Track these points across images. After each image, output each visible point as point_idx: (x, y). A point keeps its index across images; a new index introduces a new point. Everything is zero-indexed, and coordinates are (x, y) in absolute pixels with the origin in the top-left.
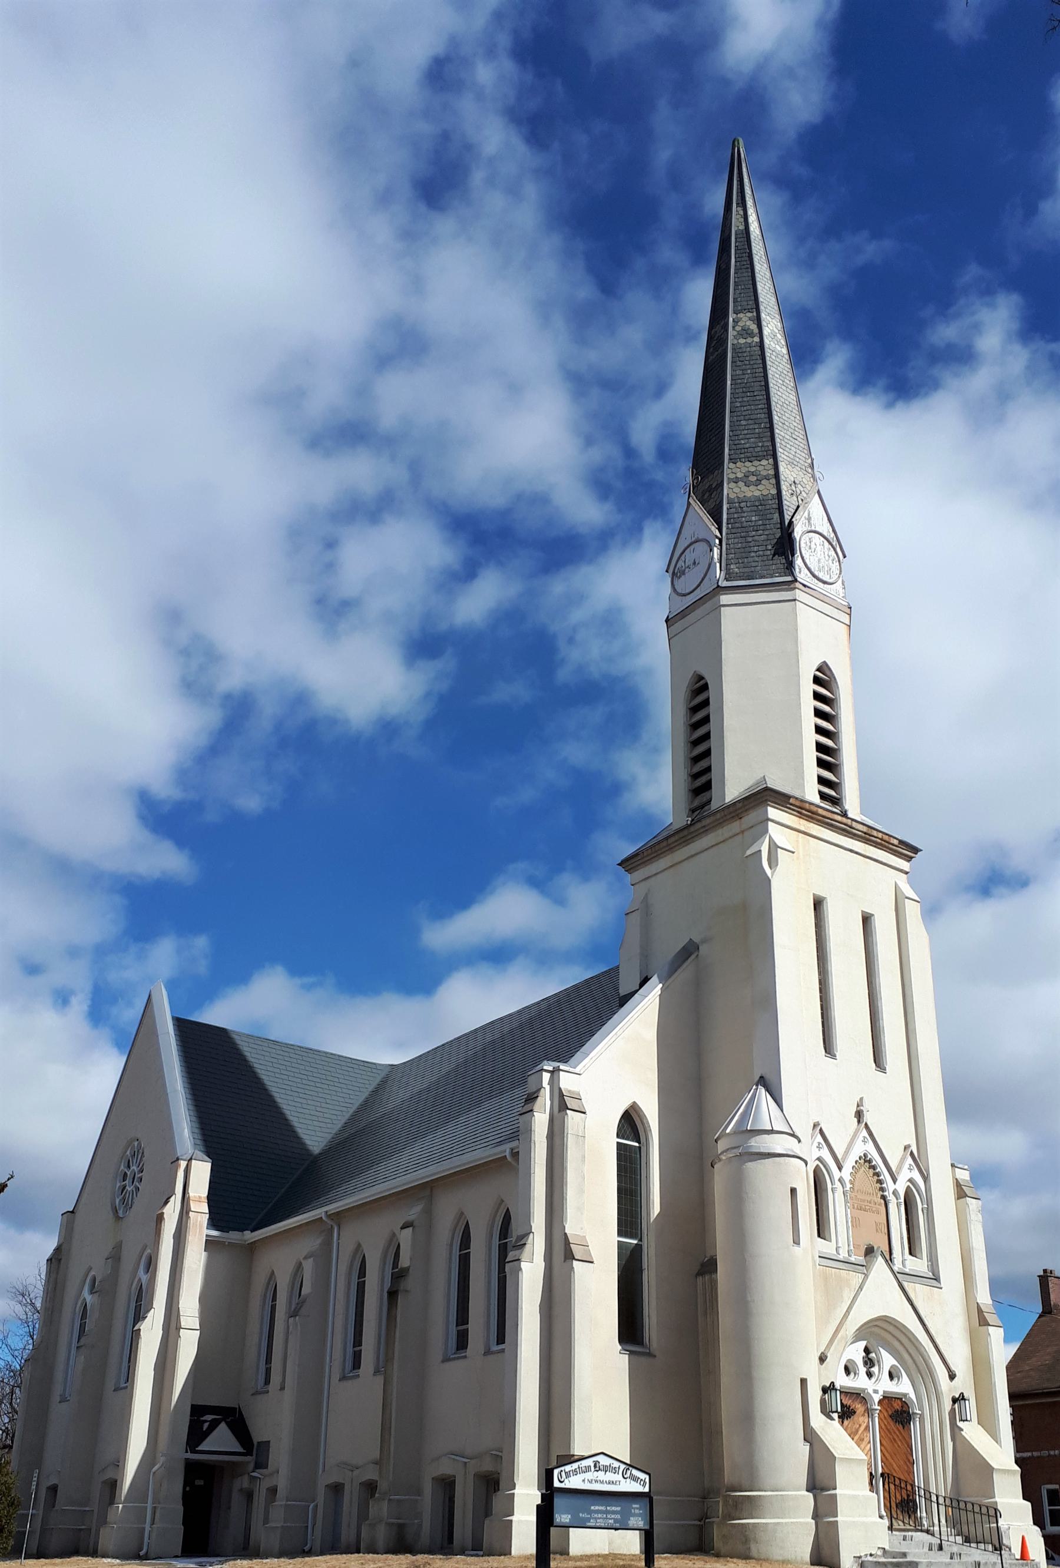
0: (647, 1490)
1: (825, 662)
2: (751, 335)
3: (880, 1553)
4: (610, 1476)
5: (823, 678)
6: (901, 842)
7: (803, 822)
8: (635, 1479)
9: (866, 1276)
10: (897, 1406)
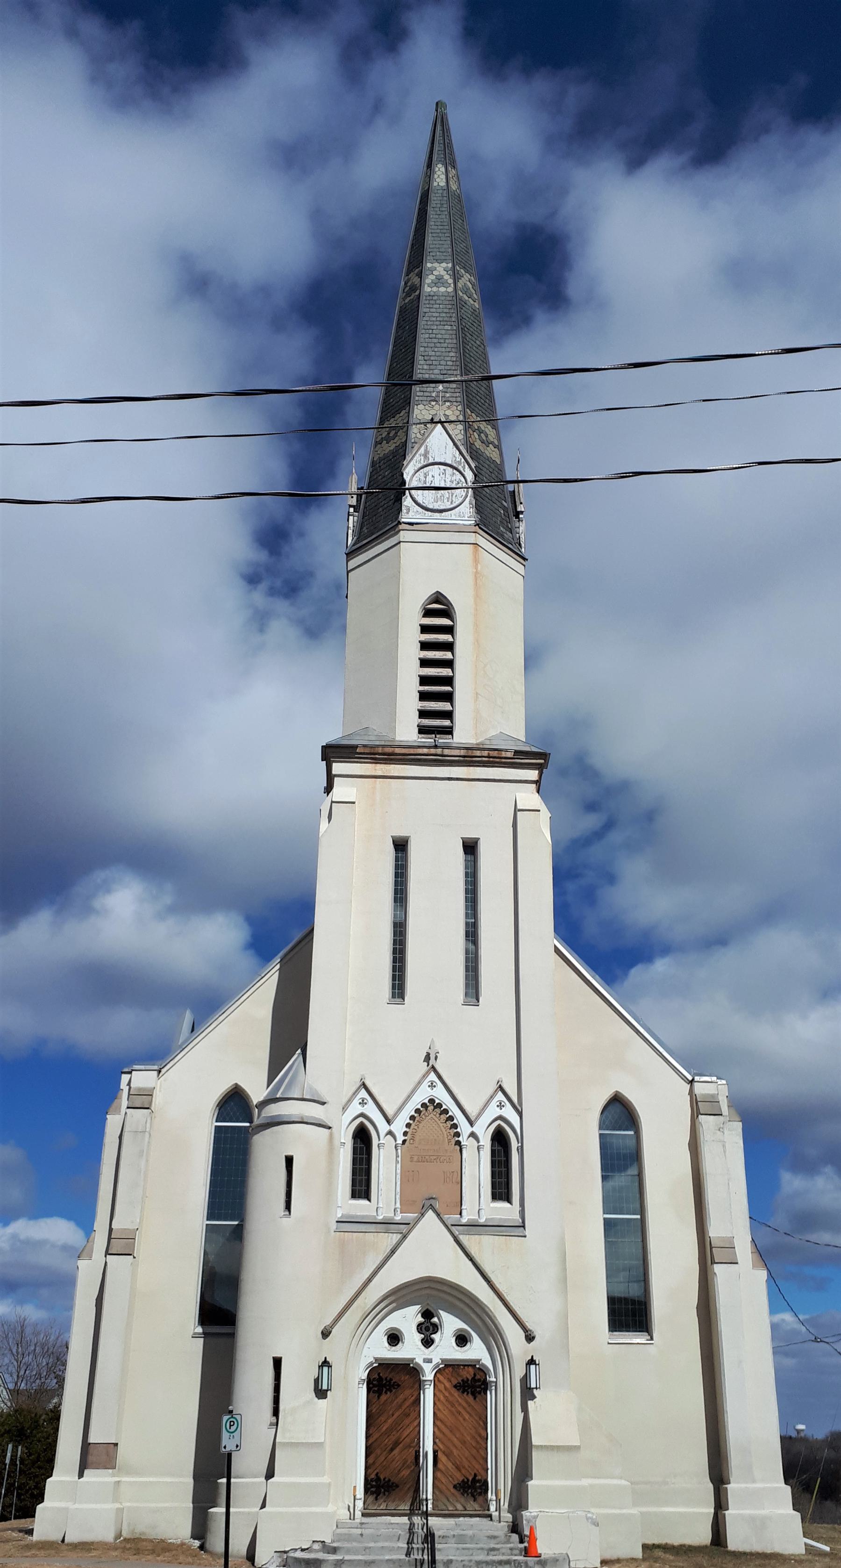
2: (445, 284)
3: (316, 1546)
5: (439, 608)
6: (517, 753)
7: (379, 766)
9: (405, 1237)
10: (468, 1374)
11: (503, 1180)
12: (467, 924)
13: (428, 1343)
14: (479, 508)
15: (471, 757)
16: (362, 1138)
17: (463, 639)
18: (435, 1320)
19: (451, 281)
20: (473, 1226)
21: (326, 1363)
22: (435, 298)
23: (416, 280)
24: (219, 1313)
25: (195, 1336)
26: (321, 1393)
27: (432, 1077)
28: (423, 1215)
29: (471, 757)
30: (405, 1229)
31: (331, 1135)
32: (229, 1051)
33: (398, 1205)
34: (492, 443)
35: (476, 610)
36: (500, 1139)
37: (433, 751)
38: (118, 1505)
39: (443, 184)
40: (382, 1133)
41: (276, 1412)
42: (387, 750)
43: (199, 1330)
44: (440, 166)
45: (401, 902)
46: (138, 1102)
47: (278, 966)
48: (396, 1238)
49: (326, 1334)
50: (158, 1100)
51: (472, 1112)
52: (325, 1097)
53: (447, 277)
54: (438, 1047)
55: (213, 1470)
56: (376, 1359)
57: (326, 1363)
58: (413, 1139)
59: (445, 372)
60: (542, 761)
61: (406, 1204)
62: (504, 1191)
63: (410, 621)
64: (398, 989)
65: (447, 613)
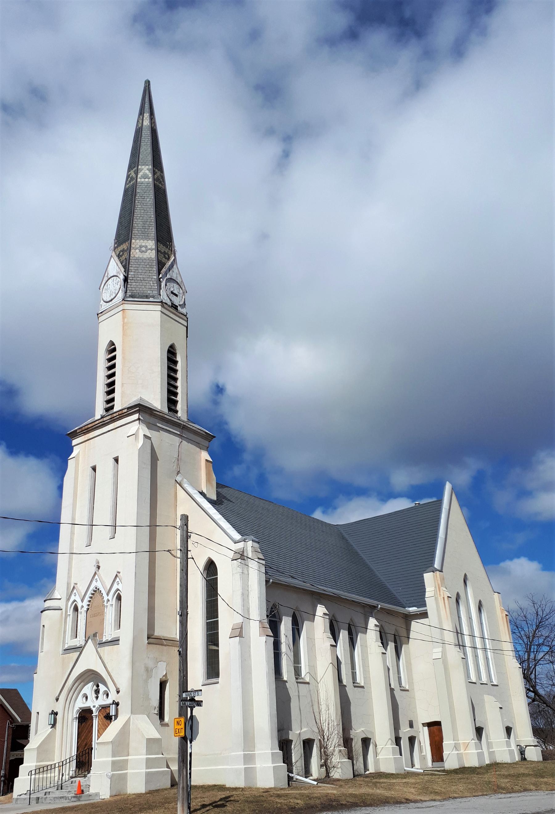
30: (80, 649)
48: (78, 653)
56: (80, 708)
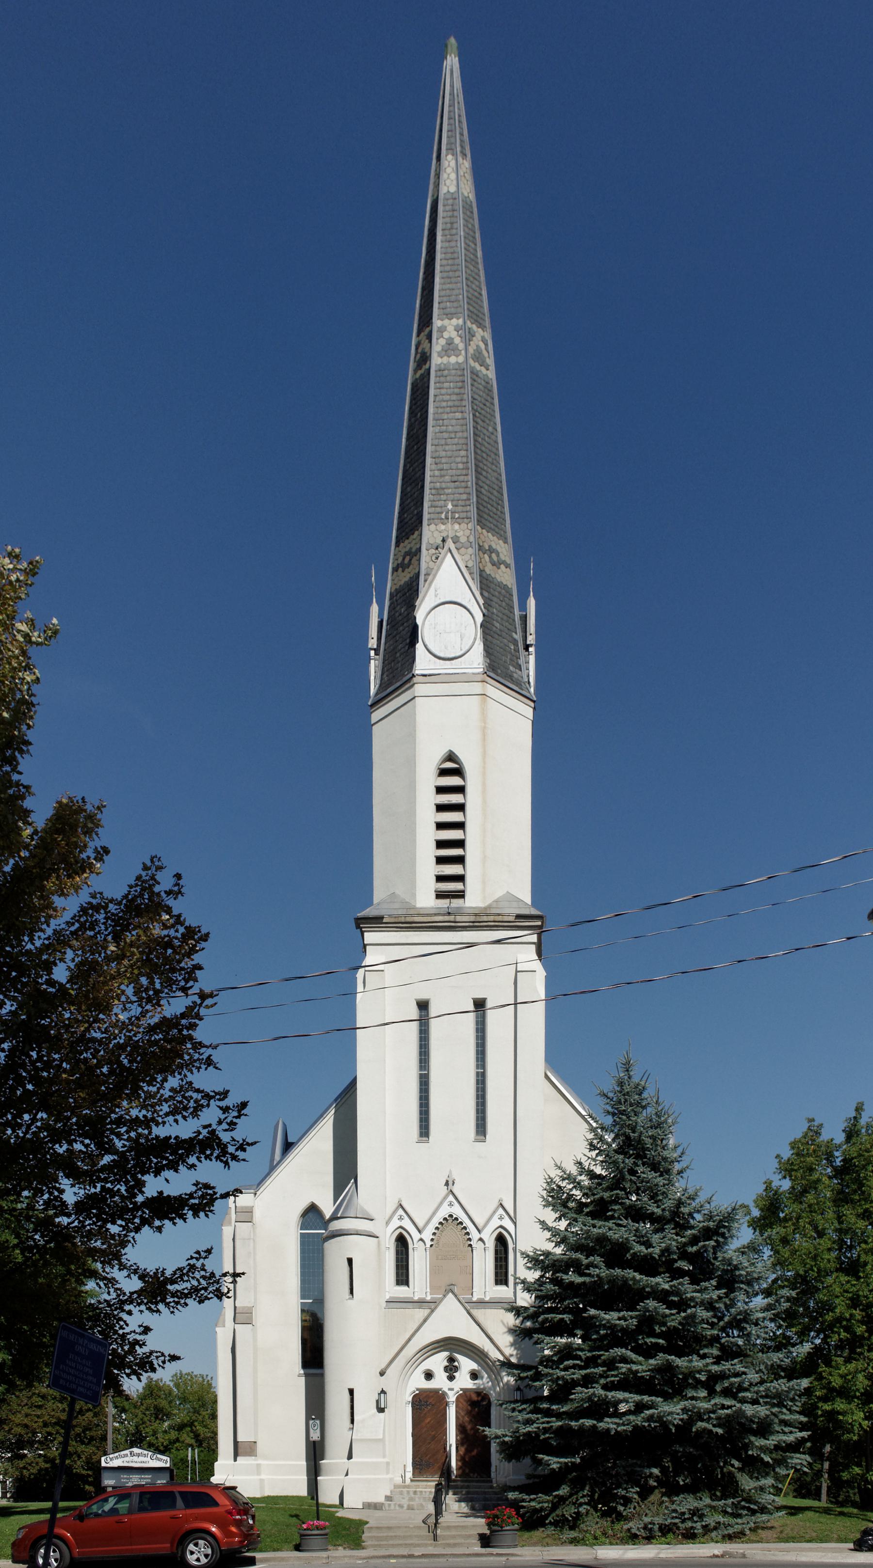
0: (168, 1465)
1: (450, 751)
4: (141, 1459)
5: (452, 767)
6: (519, 917)
8: (160, 1460)
9: (433, 1311)
11: (504, 1270)
12: (478, 1073)
13: (451, 1378)
14: (489, 651)
15: (480, 921)
16: (402, 1242)
17: (472, 799)
18: (456, 1364)
19: (461, 346)
20: (481, 1303)
21: (383, 1392)
22: (446, 372)
23: (425, 344)
24: (313, 1354)
25: (299, 1376)
26: (381, 1410)
27: (451, 1198)
28: (445, 1296)
29: (480, 921)
30: (431, 1305)
31: (379, 1242)
32: (305, 1174)
33: (428, 1290)
34: (504, 563)
35: (484, 768)
36: (501, 1241)
37: (447, 918)
38: (259, 1477)
39: (453, 189)
40: (415, 1240)
41: (352, 1422)
42: (409, 919)
43: (302, 1372)
44: (450, 157)
45: (425, 1063)
46: (243, 1217)
47: (333, 1111)
48: (427, 1311)
49: (382, 1374)
50: (257, 1215)
51: (480, 1222)
52: (373, 1214)
53: (457, 340)
54: (455, 1176)
55: (315, 1452)
57: (383, 1392)
58: (438, 1243)
59: (455, 479)
60: (539, 923)
61: (433, 1288)
62: (503, 1278)
63: (427, 780)
64: (424, 1130)
65: (458, 772)
